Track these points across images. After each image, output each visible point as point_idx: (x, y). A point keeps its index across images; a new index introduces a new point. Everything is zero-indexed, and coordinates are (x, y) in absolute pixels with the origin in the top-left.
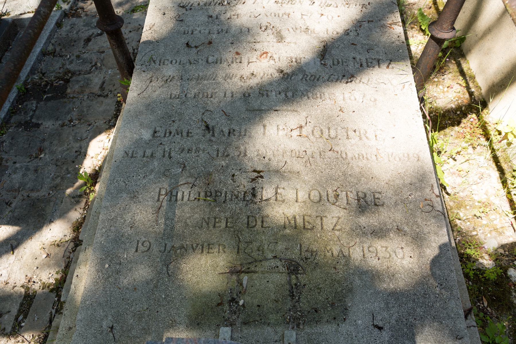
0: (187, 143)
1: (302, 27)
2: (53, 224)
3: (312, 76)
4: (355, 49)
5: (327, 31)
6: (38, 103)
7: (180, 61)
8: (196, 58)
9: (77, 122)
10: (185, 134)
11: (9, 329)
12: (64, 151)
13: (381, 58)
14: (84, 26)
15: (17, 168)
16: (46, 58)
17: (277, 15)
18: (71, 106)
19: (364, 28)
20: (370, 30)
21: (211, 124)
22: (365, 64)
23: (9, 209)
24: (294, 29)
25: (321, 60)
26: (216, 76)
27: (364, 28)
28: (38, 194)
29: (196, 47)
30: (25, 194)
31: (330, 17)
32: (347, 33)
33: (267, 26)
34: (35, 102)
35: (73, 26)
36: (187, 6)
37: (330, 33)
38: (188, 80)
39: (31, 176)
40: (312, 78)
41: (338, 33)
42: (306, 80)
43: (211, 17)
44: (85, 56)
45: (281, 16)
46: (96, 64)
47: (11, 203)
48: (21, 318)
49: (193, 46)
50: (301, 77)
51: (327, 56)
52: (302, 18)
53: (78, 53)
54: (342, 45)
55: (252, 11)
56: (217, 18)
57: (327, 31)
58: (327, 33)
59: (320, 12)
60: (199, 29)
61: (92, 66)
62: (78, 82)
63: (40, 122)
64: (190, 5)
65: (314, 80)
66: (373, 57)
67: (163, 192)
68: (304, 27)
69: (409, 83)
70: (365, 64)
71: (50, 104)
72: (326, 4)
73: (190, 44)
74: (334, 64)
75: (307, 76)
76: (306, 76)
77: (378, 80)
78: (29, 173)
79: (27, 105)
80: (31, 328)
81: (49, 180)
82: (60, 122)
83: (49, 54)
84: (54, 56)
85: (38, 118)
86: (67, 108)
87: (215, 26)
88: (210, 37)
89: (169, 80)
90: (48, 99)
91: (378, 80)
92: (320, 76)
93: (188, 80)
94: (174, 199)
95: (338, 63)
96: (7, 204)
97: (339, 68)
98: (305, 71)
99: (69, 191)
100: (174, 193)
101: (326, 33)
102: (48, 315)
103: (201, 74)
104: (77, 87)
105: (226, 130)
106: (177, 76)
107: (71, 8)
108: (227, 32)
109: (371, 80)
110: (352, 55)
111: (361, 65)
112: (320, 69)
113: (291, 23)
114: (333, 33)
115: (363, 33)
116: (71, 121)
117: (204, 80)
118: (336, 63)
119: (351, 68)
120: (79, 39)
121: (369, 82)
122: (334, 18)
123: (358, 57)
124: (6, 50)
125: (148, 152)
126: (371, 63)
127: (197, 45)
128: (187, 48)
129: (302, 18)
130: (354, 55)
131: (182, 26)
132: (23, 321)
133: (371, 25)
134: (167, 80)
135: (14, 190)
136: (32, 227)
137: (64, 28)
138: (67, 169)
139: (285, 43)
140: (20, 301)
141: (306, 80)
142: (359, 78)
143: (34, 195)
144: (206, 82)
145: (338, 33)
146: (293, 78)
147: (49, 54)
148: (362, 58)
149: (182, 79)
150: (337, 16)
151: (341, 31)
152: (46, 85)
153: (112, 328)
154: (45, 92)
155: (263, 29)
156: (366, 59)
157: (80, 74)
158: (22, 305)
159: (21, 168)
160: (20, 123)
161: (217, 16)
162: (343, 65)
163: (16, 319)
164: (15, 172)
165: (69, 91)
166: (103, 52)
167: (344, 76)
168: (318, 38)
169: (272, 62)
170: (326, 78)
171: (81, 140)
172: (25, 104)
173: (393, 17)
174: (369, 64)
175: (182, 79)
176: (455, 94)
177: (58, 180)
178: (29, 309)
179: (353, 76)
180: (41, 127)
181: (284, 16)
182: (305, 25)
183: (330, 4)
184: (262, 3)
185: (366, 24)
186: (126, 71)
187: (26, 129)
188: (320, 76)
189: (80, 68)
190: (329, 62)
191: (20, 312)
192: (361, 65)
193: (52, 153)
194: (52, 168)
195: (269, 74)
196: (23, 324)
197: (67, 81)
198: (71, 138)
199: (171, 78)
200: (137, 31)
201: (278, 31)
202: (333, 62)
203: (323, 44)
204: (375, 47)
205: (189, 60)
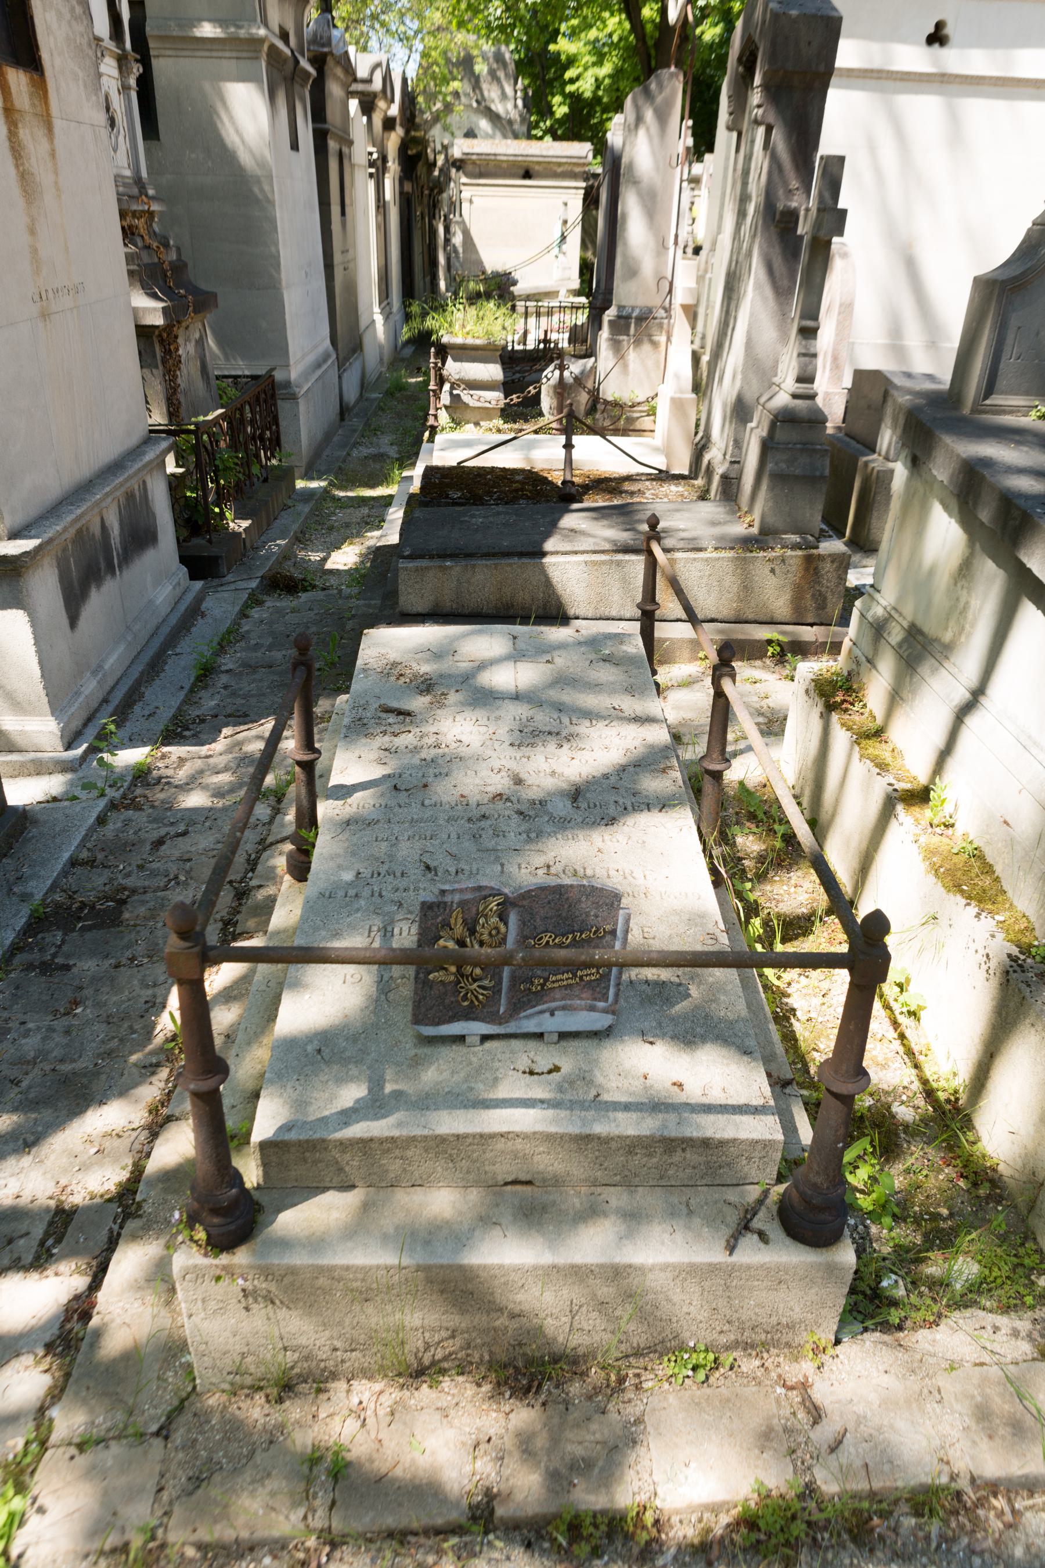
0: (403, 883)
2: (105, 1107)
6: (65, 934)
9: (146, 960)
10: (398, 874)
11: (28, 1258)
12: (123, 1002)
14: (149, 822)
15: (29, 1030)
16: (78, 870)
18: (133, 936)
21: (432, 864)
22: (630, 808)
23: (17, 1090)
28: (74, 1065)
30: (48, 1068)
32: (606, 776)
34: (60, 933)
35: (127, 823)
39: (58, 1038)
44: (154, 865)
46: (176, 877)
47: (20, 1081)
48: (50, 1242)
51: (580, 799)
53: (140, 862)
61: (170, 881)
62: (143, 903)
63: (71, 963)
67: (375, 928)
68: (548, 771)
70: (630, 808)
71: (88, 936)
78: (55, 1035)
79: (43, 938)
80: (72, 1253)
81: (94, 1045)
82: (112, 961)
83: (84, 863)
84: (92, 867)
85: (68, 956)
86: (126, 940)
88: (424, 781)
90: (89, 928)
94: (389, 934)
96: (12, 1081)
99: (134, 1058)
100: (389, 929)
102: (105, 1232)
104: (142, 910)
105: (453, 870)
107: (124, 797)
116: (132, 959)
119: (612, 810)
120: (142, 842)
123: (621, 801)
124: (5, 855)
125: (352, 892)
132: (54, 1246)
133: (638, 769)
135: (25, 1063)
136: (64, 1112)
137: (111, 826)
138: (131, 1027)
140: (47, 1218)
143: (66, 1068)
147: (84, 863)
152: (81, 908)
153: (319, 1051)
154: (79, 919)
157: (145, 892)
158: (51, 1224)
159: (39, 1028)
160: (31, 964)
163: (42, 1243)
164: (26, 1034)
165: (126, 915)
166: (189, 860)
170: (580, 820)
171: (155, 985)
172: (40, 936)
176: (807, 896)
177: (115, 1043)
178: (66, 1228)
179: (614, 819)
180: (75, 970)
185: (631, 769)
187: (43, 973)
189: (147, 883)
190: (583, 805)
191: (47, 1235)
193: (98, 1005)
194: (100, 1030)
196: (55, 1251)
197: (124, 902)
198: (135, 982)
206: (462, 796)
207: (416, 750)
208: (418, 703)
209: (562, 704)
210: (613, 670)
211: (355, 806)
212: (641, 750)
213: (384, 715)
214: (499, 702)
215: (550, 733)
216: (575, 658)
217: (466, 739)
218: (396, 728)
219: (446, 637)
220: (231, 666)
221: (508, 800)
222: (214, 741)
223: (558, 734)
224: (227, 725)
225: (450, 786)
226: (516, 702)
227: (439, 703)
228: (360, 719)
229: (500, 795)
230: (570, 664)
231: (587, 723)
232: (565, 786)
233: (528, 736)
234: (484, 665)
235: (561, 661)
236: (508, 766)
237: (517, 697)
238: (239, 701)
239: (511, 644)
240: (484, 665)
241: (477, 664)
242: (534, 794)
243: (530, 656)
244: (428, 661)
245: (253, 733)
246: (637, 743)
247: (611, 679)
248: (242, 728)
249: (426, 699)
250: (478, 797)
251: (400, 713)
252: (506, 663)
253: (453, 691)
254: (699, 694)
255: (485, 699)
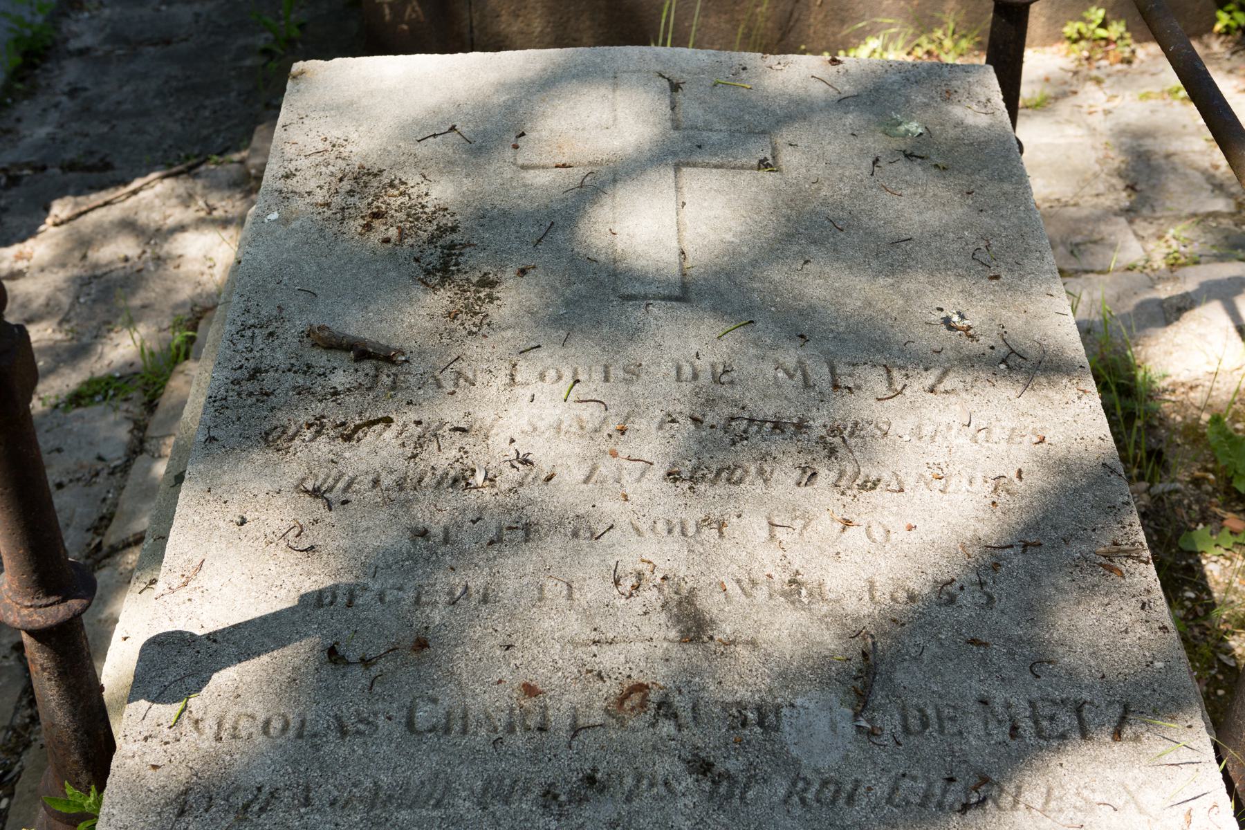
1: (776, 577)
3: (825, 783)
4: (984, 662)
5: (872, 587)
7: (303, 723)
8: (364, 708)
13: (1086, 696)
17: (677, 530)
19: (1010, 572)
20: (1035, 578)
22: (1026, 726)
24: (745, 583)
25: (856, 716)
26: (447, 788)
27: (1010, 572)
29: (366, 662)
31: (878, 534)
32: (946, 594)
33: (640, 575)
36: (330, 489)
37: (883, 591)
38: (332, 804)
40: (828, 793)
41: (912, 598)
42: (803, 800)
43: (424, 534)
45: (691, 530)
49: (352, 656)
50: (782, 792)
51: (879, 697)
52: (772, 537)
54: (934, 648)
55: (581, 511)
56: (446, 541)
57: (872, 587)
58: (872, 598)
59: (840, 513)
60: (376, 586)
64: (340, 485)
65: (833, 802)
66: (1057, 695)
69: (1206, 802)
72: (859, 482)
73: (341, 650)
74: (907, 730)
75: (808, 783)
76: (801, 785)
77: (1086, 793)
87: (440, 575)
89: (256, 808)
91: (1086, 793)
92: (857, 783)
93: (332, 804)
95: (925, 724)
97: (930, 744)
98: (796, 761)
101: (867, 597)
103: (385, 779)
106: (288, 787)
108: (485, 600)
109: (1056, 793)
110: (977, 688)
111: (1014, 731)
112: (855, 754)
113: (732, 559)
114: (893, 599)
115: (1009, 596)
117: (400, 806)
118: (914, 723)
119: (976, 740)
121: (1053, 804)
122: (893, 536)
123: (999, 696)
126: (1052, 718)
127: (372, 653)
128: (330, 666)
129: (772, 537)
130: (983, 689)
131: (309, 574)
134: (246, 807)
139: (712, 646)
141: (803, 800)
142: (1010, 788)
144: (404, 814)
145: (912, 598)
146: (751, 794)
148: (1013, 697)
149: (307, 802)
150: (904, 526)
151: (926, 590)
155: (627, 585)
156: (1032, 704)
161: (446, 530)
162: (941, 730)
167: (951, 780)
168: (839, 618)
169: (667, 728)
173: (1116, 526)
174: (1045, 723)
175: (307, 802)
181: (705, 530)
182: (784, 568)
183: (873, 477)
184: (618, 481)
185: (1016, 559)
186: (76, 757)
188: (857, 783)
190: (889, 722)
192: (1014, 731)
195: (660, 779)
199: (263, 797)
200: (89, 484)
201: (684, 592)
202: (904, 718)
203: (859, 644)
204: (1061, 650)
205: (338, 718)
206: (530, 690)
207: (405, 489)
208: (415, 317)
209: (809, 312)
210: (937, 188)
211: (209, 727)
212: (1037, 479)
213: (321, 359)
214: (635, 313)
215: (778, 426)
216: (833, 149)
217: (543, 457)
218: (349, 411)
219: (502, 86)
220: (88, 40)
221: (665, 708)
222: (32, 233)
223: (801, 426)
224: (61, 192)
225: (492, 645)
226: (683, 311)
227: (472, 319)
228: (255, 374)
229: (640, 688)
230: (819, 170)
231: (875, 381)
232: (828, 639)
233: (724, 444)
234: (599, 182)
235: (803, 158)
236: (664, 567)
237: (684, 291)
238: (97, 128)
239: (664, 107)
240: (599, 182)
241: (576, 175)
242: (742, 679)
243: (716, 149)
244: (448, 166)
245: (115, 212)
246: (1022, 455)
247: (934, 218)
248: (96, 198)
249: (440, 300)
250: (575, 696)
251: (362, 352)
252: (653, 175)
253: (511, 271)
254: (1071, 131)
255: (599, 301)
